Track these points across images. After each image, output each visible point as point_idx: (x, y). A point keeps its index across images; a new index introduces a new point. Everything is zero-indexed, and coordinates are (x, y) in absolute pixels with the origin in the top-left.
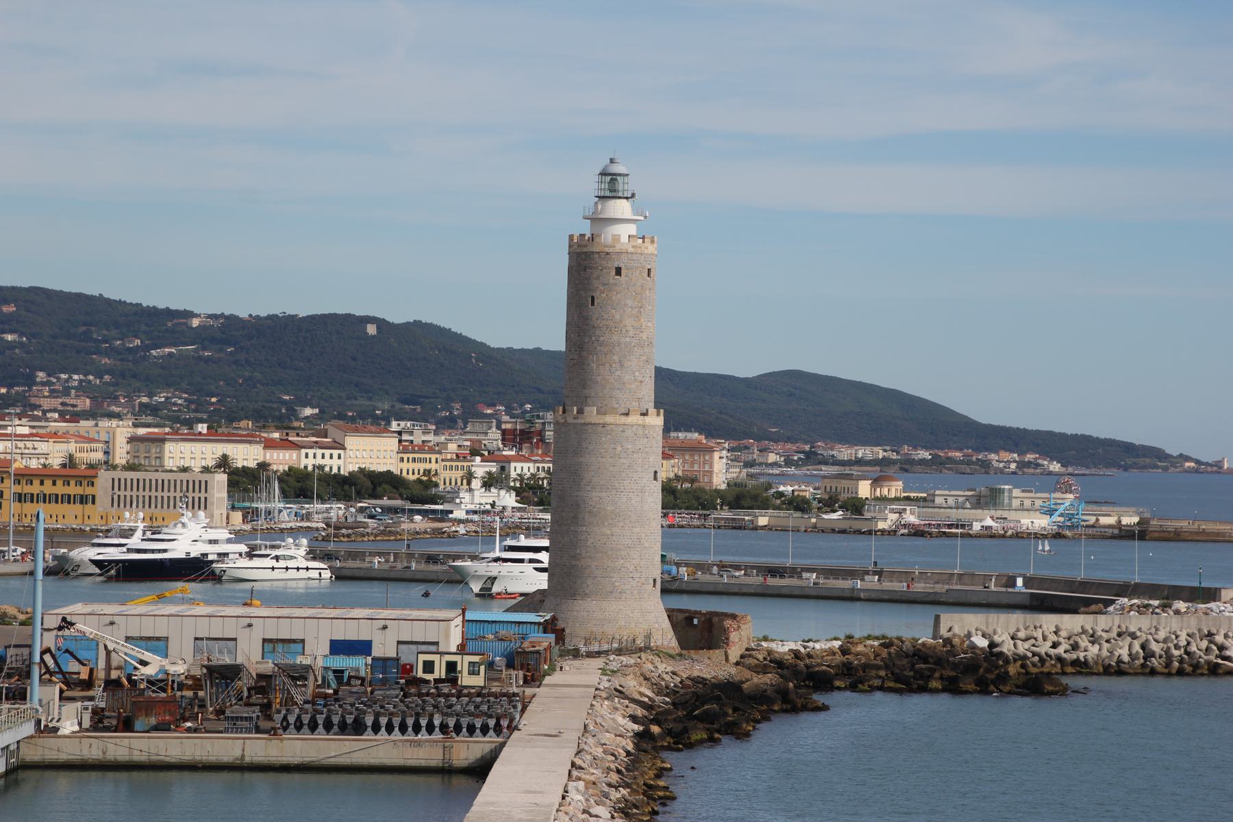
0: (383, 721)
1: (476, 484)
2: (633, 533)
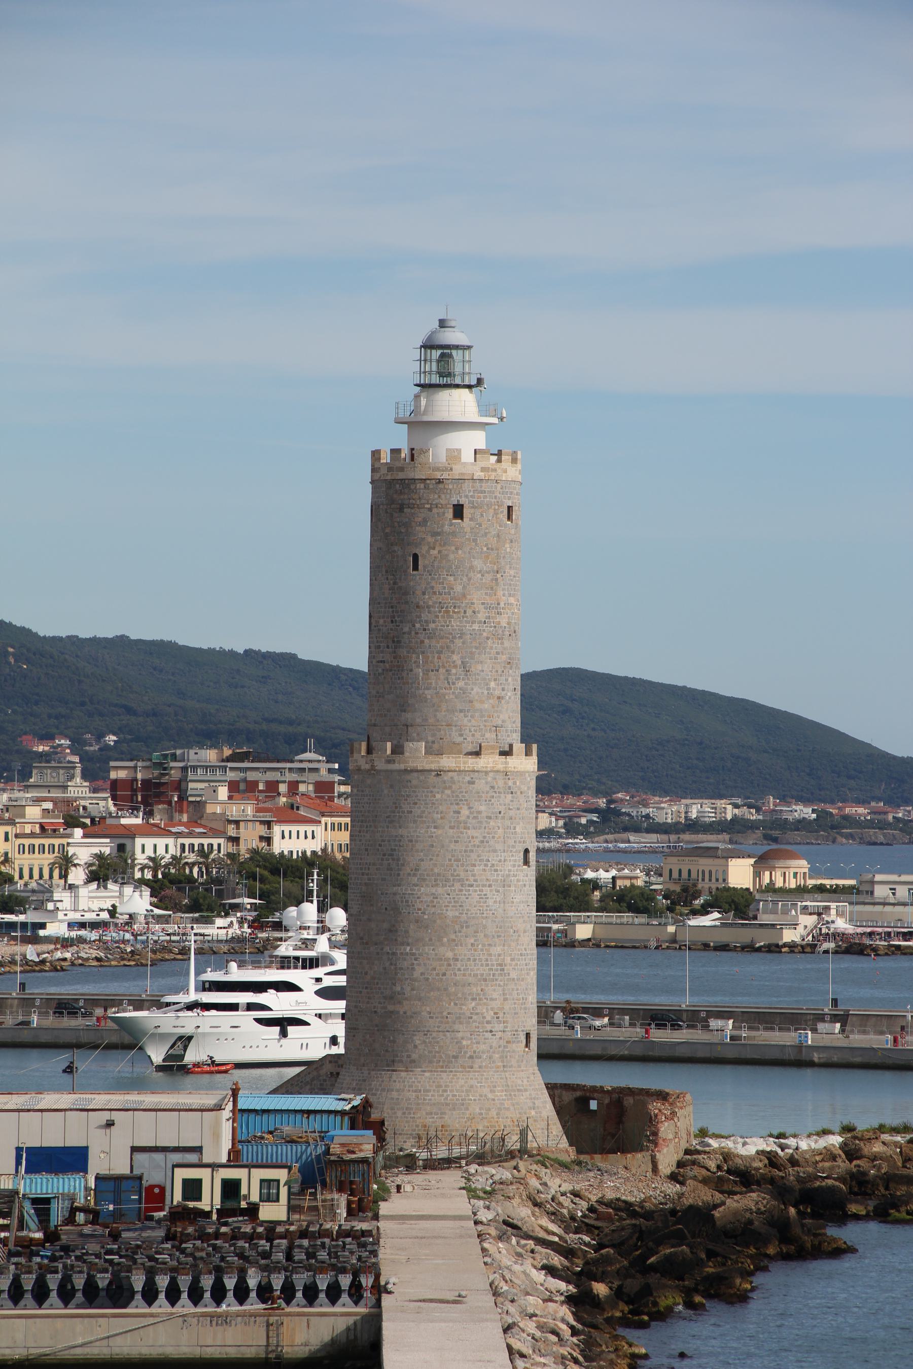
0: (162, 1282)
1: (77, 876)
2: (490, 955)
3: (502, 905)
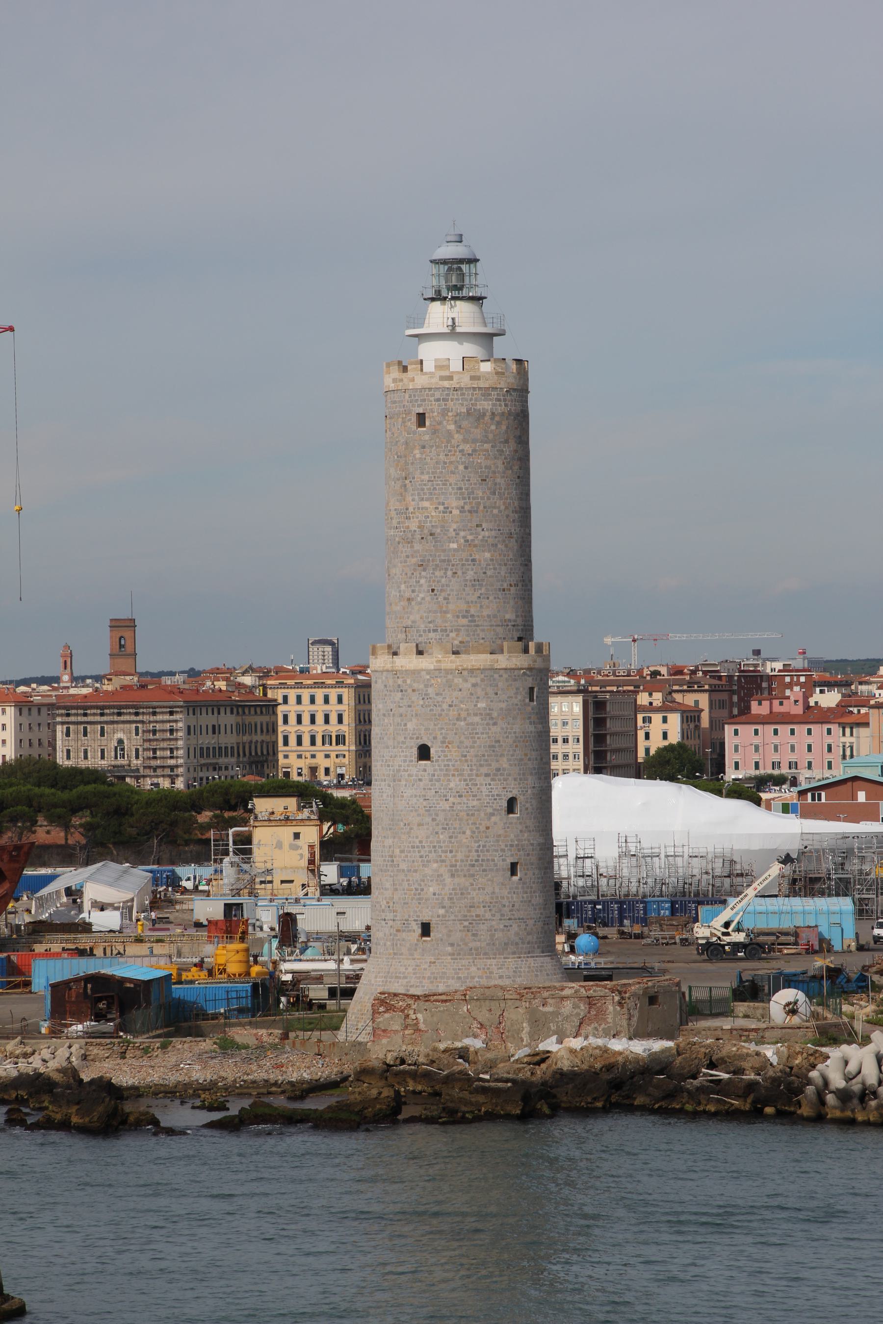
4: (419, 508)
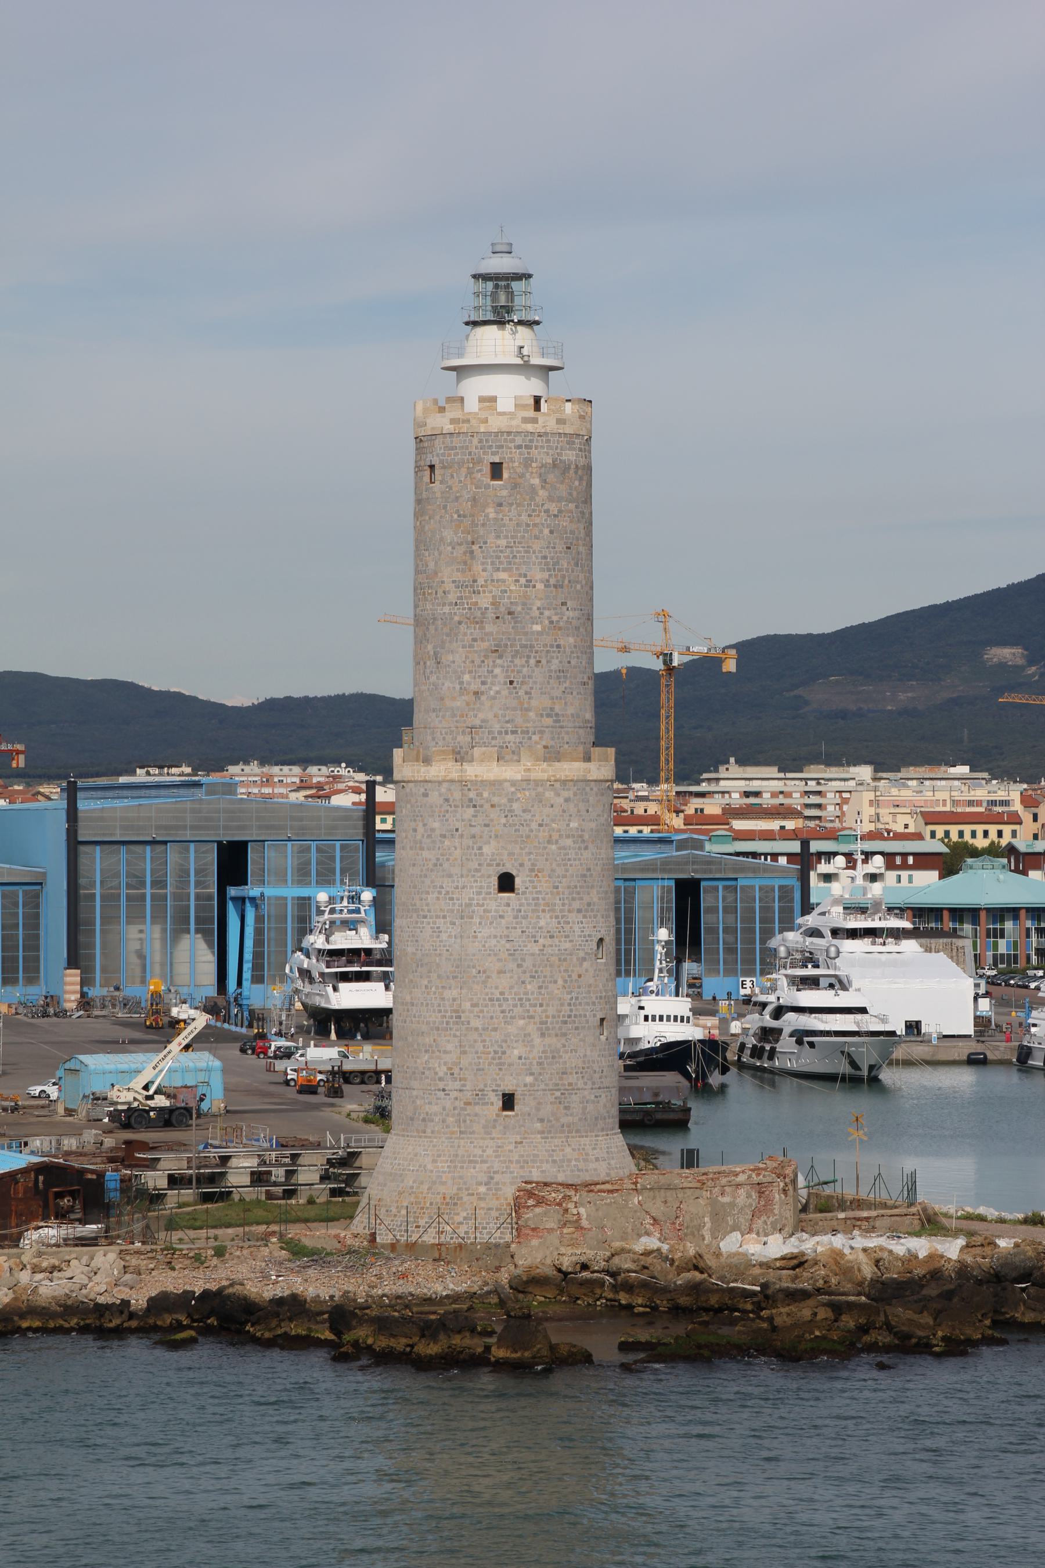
2: (443, 999)
3: (459, 940)
4: (493, 581)
